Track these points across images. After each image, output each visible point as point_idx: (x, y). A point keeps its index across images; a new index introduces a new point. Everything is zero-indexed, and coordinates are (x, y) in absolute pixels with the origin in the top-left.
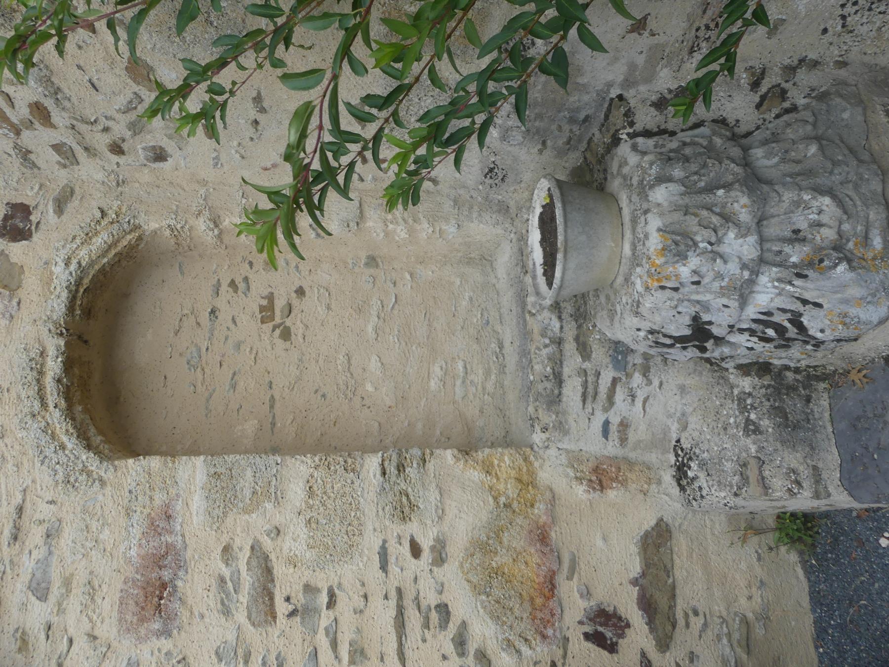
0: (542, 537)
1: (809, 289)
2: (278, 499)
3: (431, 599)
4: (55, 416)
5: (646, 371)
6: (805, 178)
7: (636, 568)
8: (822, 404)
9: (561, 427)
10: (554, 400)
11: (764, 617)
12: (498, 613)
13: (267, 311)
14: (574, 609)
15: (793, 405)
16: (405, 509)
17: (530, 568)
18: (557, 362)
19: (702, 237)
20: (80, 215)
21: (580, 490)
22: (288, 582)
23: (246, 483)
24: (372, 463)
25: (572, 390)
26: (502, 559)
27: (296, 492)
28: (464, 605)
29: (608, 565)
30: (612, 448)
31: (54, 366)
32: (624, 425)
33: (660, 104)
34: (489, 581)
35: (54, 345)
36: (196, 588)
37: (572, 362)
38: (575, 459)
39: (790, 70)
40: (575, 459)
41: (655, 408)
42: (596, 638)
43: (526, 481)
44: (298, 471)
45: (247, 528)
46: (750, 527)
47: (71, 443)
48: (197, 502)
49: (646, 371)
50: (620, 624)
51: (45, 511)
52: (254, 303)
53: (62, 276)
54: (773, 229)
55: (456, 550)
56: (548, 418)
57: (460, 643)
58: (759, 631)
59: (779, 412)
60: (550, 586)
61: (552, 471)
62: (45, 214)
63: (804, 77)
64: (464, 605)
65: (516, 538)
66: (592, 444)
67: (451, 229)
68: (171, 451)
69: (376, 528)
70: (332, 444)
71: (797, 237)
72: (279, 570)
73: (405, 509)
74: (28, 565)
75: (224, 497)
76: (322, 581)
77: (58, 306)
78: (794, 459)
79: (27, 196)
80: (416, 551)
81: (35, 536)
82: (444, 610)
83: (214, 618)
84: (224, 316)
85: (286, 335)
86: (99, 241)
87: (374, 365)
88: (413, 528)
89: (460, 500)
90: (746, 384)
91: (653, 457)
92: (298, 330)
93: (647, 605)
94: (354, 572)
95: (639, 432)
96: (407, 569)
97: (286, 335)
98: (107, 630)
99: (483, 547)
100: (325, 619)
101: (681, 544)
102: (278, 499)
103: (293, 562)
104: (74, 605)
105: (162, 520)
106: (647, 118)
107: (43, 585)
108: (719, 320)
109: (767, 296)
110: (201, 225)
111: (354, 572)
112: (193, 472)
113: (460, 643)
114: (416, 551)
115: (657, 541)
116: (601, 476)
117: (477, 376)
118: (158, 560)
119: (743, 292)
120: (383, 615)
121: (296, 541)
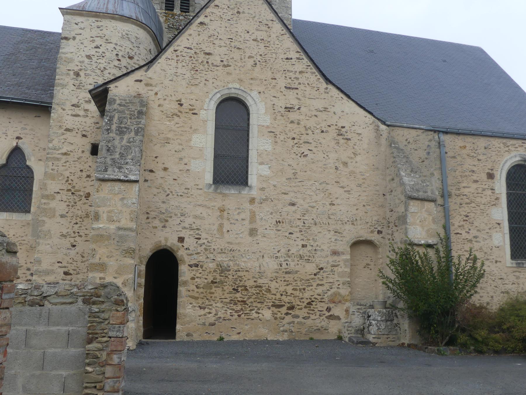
0: (340, 302)
1: (375, 326)
2: (345, 268)
3: (333, 287)
4: (355, 240)
5: (362, 316)
6: (387, 326)
7: (335, 315)
8: (359, 336)
9: (354, 305)
10: (358, 304)
11: (328, 333)
12: (331, 295)
13: (368, 264)
14: (331, 305)
15: (359, 332)
16: (344, 284)
17: (336, 300)
18: (363, 305)
19: (380, 314)
20: (381, 240)
21: (345, 308)
22: (335, 269)
23: (347, 263)
24: (349, 280)
25: (359, 307)
26: (338, 296)
27: (346, 270)
28: (332, 291)
29: (337, 311)
30: (351, 313)
31: (361, 239)
32: (354, 314)
33: (395, 313)
34: (335, 294)
35: (364, 239)
36: (335, 258)
37: (363, 307)
38: (349, 307)
39: (399, 327)
40: (349, 307)
41: (356, 319)
42: (327, 308)
43: (346, 301)
44: (348, 270)
45: (342, 264)
46: (340, 332)
47: (352, 242)
48: (345, 257)
49: (362, 316)
50: (329, 311)
51: (344, 240)
52: (369, 263)
53: (373, 239)
54: (381, 322)
55: (339, 290)
56: (355, 304)
57: (328, 290)
58: (327, 331)
59: (358, 330)
60: (334, 302)
61: (348, 304)
62: (381, 235)
63: (399, 329)
64: (332, 291)
65: (340, 298)
66: (351, 310)
67: (381, 292)
68: (351, 254)
69: (342, 280)
70: (351, 275)
71: (380, 325)
72: (337, 268)
73: (344, 284)
74: (338, 238)
75: (346, 261)
76: (335, 273)
77: (369, 239)
78: (353, 331)
79: (383, 233)
80: (339, 285)
81: (341, 239)
82: (332, 288)
83: (332, 260)
84: (367, 258)
85: (365, 267)
86: (378, 243)
87: (360, 280)
88: (341, 285)
89: (344, 291)
90: (362, 327)
91: (349, 319)
92: (365, 269)
93: (331, 316)
94: (336, 278)
95: (353, 317)
96: (336, 284)
97: (365, 267)
98: (331, 248)
99: (339, 294)
100: (331, 273)
101: (338, 321)
102: (345, 268)
103: (338, 269)
104: (334, 244)
105: (343, 253)
106: (394, 312)
107: (462, 338)
108: (371, 318)
109: (374, 322)
110: (380, 256)
111: (336, 278)
112: (348, 257)
113: (328, 290)
114: (339, 285)
115: (338, 318)
116: (347, 311)
117: (359, 296)
118: (338, 253)
119: (374, 320)
120: (331, 281)
121: (340, 270)
